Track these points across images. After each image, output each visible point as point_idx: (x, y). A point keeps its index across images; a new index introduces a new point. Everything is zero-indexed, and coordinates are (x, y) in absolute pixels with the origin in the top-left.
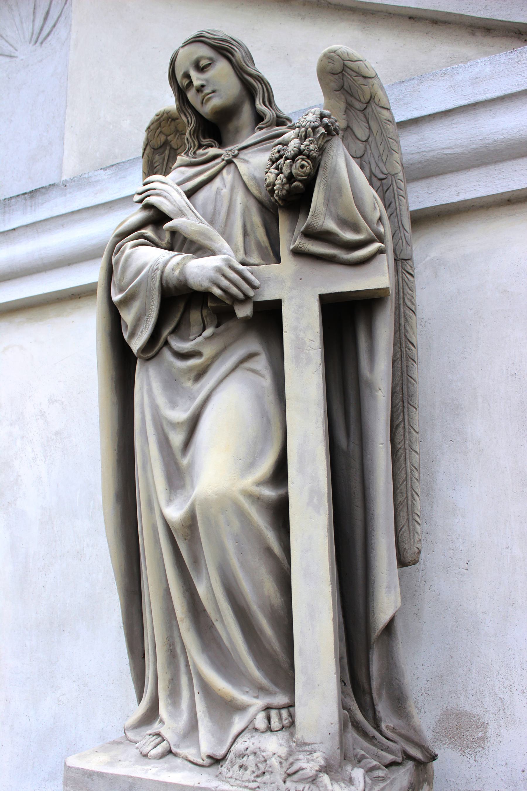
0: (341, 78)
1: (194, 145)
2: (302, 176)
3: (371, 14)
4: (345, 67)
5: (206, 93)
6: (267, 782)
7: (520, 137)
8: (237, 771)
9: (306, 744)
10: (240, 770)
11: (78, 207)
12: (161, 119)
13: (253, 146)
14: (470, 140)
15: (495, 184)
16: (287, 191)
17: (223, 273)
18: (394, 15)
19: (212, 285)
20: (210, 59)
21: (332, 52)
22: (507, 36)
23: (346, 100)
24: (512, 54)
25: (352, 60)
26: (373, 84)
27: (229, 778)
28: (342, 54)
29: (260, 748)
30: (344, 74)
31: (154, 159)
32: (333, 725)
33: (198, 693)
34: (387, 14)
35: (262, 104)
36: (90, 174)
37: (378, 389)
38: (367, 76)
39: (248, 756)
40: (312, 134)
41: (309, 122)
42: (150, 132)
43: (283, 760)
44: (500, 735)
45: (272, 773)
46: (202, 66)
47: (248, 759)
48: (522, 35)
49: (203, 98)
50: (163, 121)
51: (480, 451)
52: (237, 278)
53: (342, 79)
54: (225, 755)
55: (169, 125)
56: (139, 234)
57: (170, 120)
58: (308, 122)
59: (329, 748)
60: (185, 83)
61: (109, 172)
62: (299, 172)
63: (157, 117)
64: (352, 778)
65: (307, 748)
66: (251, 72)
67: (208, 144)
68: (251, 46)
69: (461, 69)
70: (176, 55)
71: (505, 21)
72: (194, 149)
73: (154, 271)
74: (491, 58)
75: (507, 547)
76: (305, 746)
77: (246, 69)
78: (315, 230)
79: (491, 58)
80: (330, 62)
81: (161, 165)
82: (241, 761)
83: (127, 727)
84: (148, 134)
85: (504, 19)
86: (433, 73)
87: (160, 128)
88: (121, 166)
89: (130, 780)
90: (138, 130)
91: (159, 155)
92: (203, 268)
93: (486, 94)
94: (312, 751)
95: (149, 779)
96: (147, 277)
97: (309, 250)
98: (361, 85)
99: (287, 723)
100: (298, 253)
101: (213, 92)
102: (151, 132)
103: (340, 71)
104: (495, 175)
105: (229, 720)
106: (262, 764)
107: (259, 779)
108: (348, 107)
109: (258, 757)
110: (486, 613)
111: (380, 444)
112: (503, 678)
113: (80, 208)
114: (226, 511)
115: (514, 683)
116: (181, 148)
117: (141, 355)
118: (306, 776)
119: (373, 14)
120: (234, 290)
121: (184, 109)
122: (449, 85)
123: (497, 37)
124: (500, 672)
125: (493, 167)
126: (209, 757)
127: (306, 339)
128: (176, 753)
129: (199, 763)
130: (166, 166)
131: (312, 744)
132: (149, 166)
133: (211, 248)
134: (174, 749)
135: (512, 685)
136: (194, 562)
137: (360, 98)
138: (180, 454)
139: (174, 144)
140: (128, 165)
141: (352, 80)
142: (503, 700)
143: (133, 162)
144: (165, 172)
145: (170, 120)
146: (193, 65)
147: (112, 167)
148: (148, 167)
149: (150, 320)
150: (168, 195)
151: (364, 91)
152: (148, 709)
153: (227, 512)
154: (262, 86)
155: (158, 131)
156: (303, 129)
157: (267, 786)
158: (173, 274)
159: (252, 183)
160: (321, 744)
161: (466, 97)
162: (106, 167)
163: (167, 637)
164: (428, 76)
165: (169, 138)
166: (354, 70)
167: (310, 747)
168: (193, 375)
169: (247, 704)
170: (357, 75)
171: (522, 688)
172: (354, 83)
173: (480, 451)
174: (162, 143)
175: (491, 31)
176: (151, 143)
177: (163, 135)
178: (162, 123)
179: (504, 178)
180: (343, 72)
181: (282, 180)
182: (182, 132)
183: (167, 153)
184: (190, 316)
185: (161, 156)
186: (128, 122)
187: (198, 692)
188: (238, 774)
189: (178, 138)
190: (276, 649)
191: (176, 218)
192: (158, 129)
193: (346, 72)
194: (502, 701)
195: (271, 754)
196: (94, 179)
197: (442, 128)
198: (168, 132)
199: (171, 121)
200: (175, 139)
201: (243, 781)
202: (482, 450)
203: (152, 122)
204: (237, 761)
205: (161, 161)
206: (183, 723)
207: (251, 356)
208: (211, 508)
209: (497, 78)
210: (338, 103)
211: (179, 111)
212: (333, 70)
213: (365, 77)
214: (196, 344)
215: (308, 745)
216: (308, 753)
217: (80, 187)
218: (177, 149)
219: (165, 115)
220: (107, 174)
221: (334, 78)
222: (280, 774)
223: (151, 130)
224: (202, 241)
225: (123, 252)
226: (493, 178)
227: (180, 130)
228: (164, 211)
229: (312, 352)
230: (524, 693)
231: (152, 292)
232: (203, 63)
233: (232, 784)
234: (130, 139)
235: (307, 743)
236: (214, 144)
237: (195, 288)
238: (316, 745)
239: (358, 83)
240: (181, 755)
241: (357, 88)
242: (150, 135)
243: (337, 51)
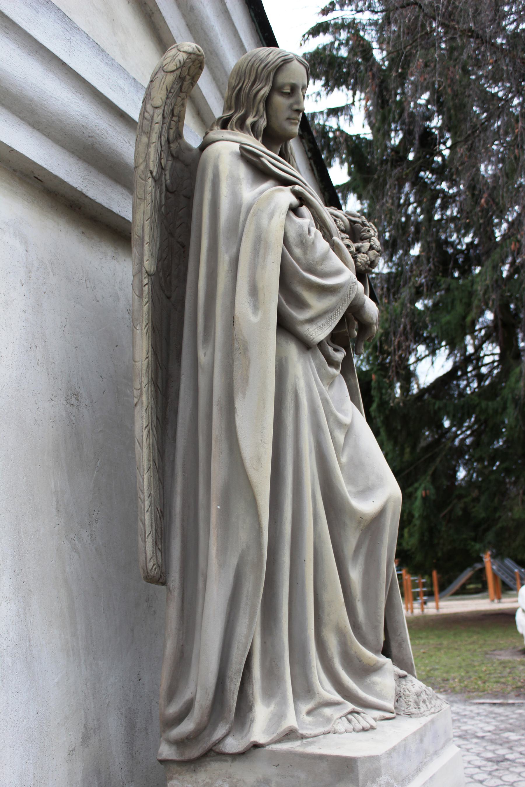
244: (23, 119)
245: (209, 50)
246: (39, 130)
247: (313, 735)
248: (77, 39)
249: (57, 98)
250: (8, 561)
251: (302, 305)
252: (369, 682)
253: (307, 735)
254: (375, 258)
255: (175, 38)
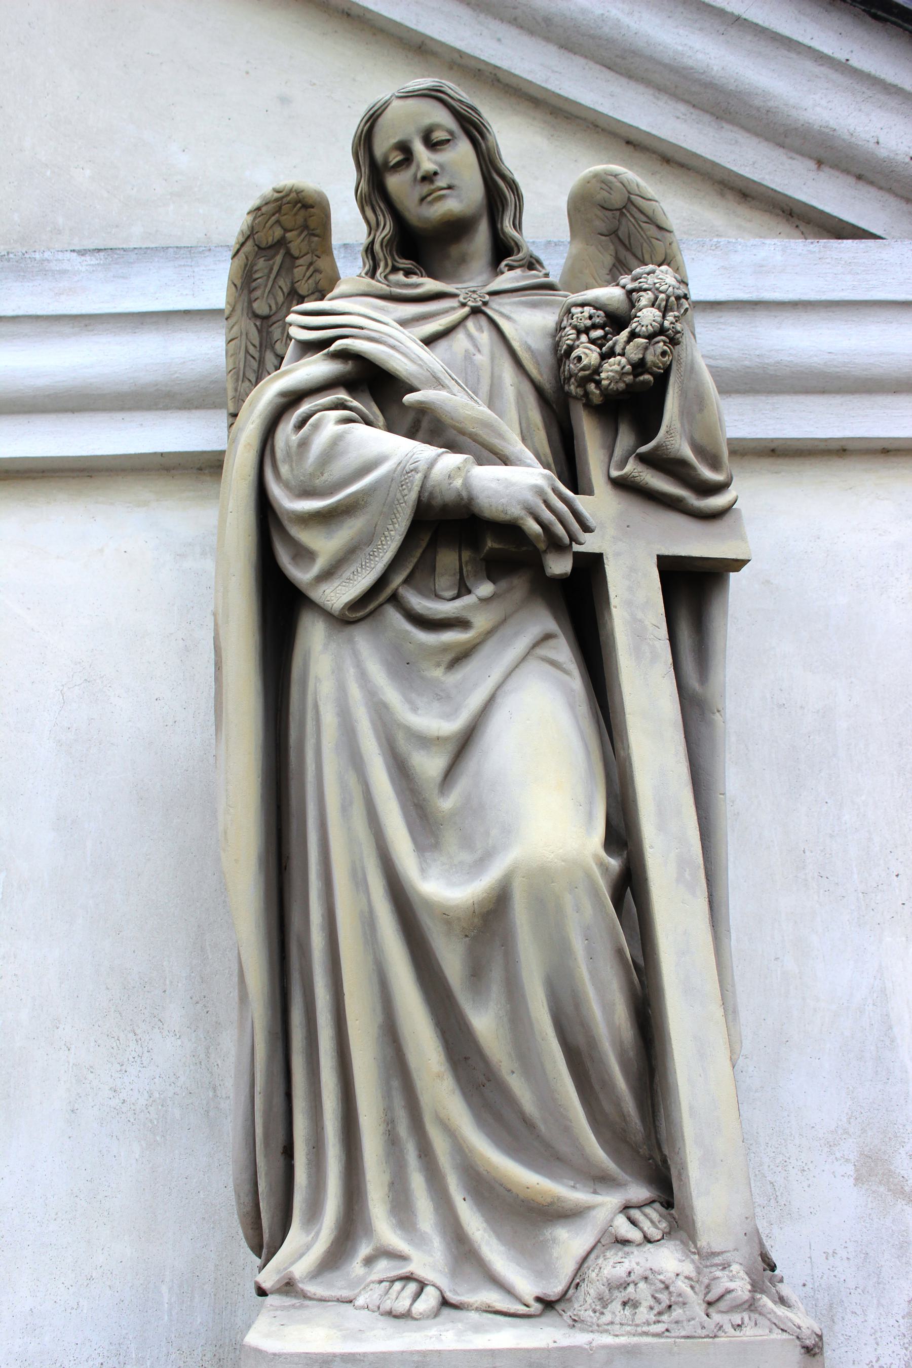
0: (618, 218)
1: (386, 265)
2: (659, 368)
3: (565, 117)
4: (629, 204)
5: (438, 187)
6: (681, 1319)
7: (813, 365)
8: (619, 1312)
9: (714, 1254)
10: (624, 1309)
11: (14, 310)
12: (285, 200)
13: (510, 294)
14: (743, 352)
15: (765, 423)
16: (627, 385)
17: (545, 498)
18: (602, 130)
19: (526, 515)
20: (451, 133)
21: (612, 175)
22: (771, 213)
23: (616, 253)
24: (812, 246)
25: (645, 196)
26: (672, 242)
27: (608, 1324)
28: (629, 183)
29: (651, 1269)
30: (624, 213)
31: (255, 264)
32: (749, 1220)
33: (464, 1200)
34: (591, 126)
35: (512, 227)
36: (47, 255)
37: (716, 711)
38: (664, 226)
39: (636, 1284)
40: (676, 307)
41: (667, 286)
42: (259, 216)
43: (694, 1282)
44: (770, 1237)
45: (684, 1304)
46: (435, 141)
47: (636, 1288)
48: (792, 217)
49: (430, 192)
50: (288, 203)
51: (735, 814)
52: (566, 511)
53: (619, 221)
54: (563, 1293)
55: (296, 214)
56: (338, 401)
57: (299, 205)
58: (670, 286)
59: (747, 1256)
60: (394, 158)
61: (91, 260)
62: (657, 361)
63: (276, 195)
64: (783, 1297)
65: (717, 1260)
66: (505, 172)
67: (408, 268)
68: (349, 107)
69: (740, 247)
70: (383, 108)
71: (779, 193)
72: (384, 271)
73: (408, 473)
74: (784, 243)
75: (777, 959)
76: (713, 1258)
77: (499, 165)
78: (667, 455)
79: (784, 243)
80: (603, 189)
81: (265, 277)
82: (623, 1294)
83: (300, 1278)
84: (255, 219)
85: (778, 189)
86: (698, 241)
87: (277, 215)
88: (118, 254)
89: (416, 1358)
90: (109, 192)
91: (264, 261)
92: (509, 484)
93: (775, 292)
94: (724, 1264)
95: (457, 1350)
96: (390, 480)
97: (647, 484)
98: (652, 237)
99: (665, 1228)
100: (623, 485)
101: (450, 187)
102: (262, 217)
103: (619, 205)
104: (766, 410)
105: (534, 1238)
106: (662, 1293)
107: (665, 1318)
108: (617, 264)
109: (652, 1284)
110: (747, 1056)
111: (720, 794)
112: (774, 1152)
113: (20, 312)
114: (576, 888)
115: (789, 1158)
116: (305, 257)
117: (347, 613)
118: (739, 1302)
119: (567, 118)
120: (560, 530)
121: (373, 199)
122: (722, 264)
123: (756, 209)
124: (769, 1143)
125: (763, 398)
126: (539, 1299)
127: (647, 623)
128: (461, 1303)
129: (521, 1312)
130: (273, 282)
131: (722, 1253)
132: (245, 276)
133: (502, 451)
134: (452, 1297)
135: (787, 1160)
136: (472, 976)
137: (643, 257)
138: (436, 791)
139: (294, 248)
140: (133, 256)
141: (637, 226)
142: (775, 1184)
143: (145, 253)
144: (269, 292)
145: (299, 205)
146: (422, 134)
147: (98, 252)
148: (243, 276)
149: (381, 554)
150: (401, 345)
151: (654, 247)
152: (332, 1242)
153: (576, 889)
154: (515, 198)
155: (274, 218)
156: (662, 296)
157: (683, 1326)
158: (450, 484)
159: (527, 356)
160: (736, 1252)
161: (745, 288)
162: (85, 250)
163: (384, 1110)
164: (691, 243)
165: (289, 235)
166: (645, 212)
167: (720, 1258)
168: (448, 657)
169: (586, 1205)
170: (648, 221)
171: (801, 1164)
172: (639, 232)
173: (735, 814)
174: (275, 240)
175: (749, 199)
176: (256, 236)
177: (279, 228)
178: (283, 207)
179: (778, 417)
180: (624, 210)
181: (624, 367)
182: (314, 232)
183: (279, 259)
184: (438, 558)
185: (267, 262)
186: (88, 172)
187: (463, 1197)
188: (624, 1316)
189: (304, 239)
190: (629, 1112)
191: (424, 389)
192: (274, 215)
193: (629, 212)
194: (773, 1186)
195: (673, 1276)
196: (54, 266)
197: (703, 325)
198: (289, 225)
199: (301, 208)
200: (299, 240)
201: (637, 1325)
202: (738, 813)
203: (268, 201)
204: (615, 1295)
205: (266, 271)
206: (439, 1253)
207: (548, 637)
208: (553, 882)
209: (791, 273)
210: (602, 254)
211: (364, 202)
212: (605, 202)
213: (660, 228)
214: (465, 608)
215: (718, 1256)
216: (720, 1268)
217: (22, 274)
218: (297, 258)
219: (293, 195)
220: (85, 263)
221: (604, 215)
222: (699, 1304)
223: (263, 215)
224: (485, 436)
225: (316, 427)
226: (763, 414)
227: (312, 227)
228: (397, 370)
229: (658, 644)
230: (804, 1170)
231: (396, 508)
232: (438, 135)
233: (617, 1333)
234: (90, 206)
235: (715, 1252)
236: (418, 272)
237: (487, 514)
238: (729, 1254)
239: (647, 233)
240: (471, 1306)
241: (642, 240)
242: (259, 222)
243: (620, 176)
244: (166, 408)
245: (617, 56)
246: (197, 408)
247: (318, 1296)
248: (206, 266)
249: (193, 358)
250: (180, 985)
251: (303, 554)
252: (549, 1237)
253: (309, 1294)
254: (644, 355)
255: (543, 85)
